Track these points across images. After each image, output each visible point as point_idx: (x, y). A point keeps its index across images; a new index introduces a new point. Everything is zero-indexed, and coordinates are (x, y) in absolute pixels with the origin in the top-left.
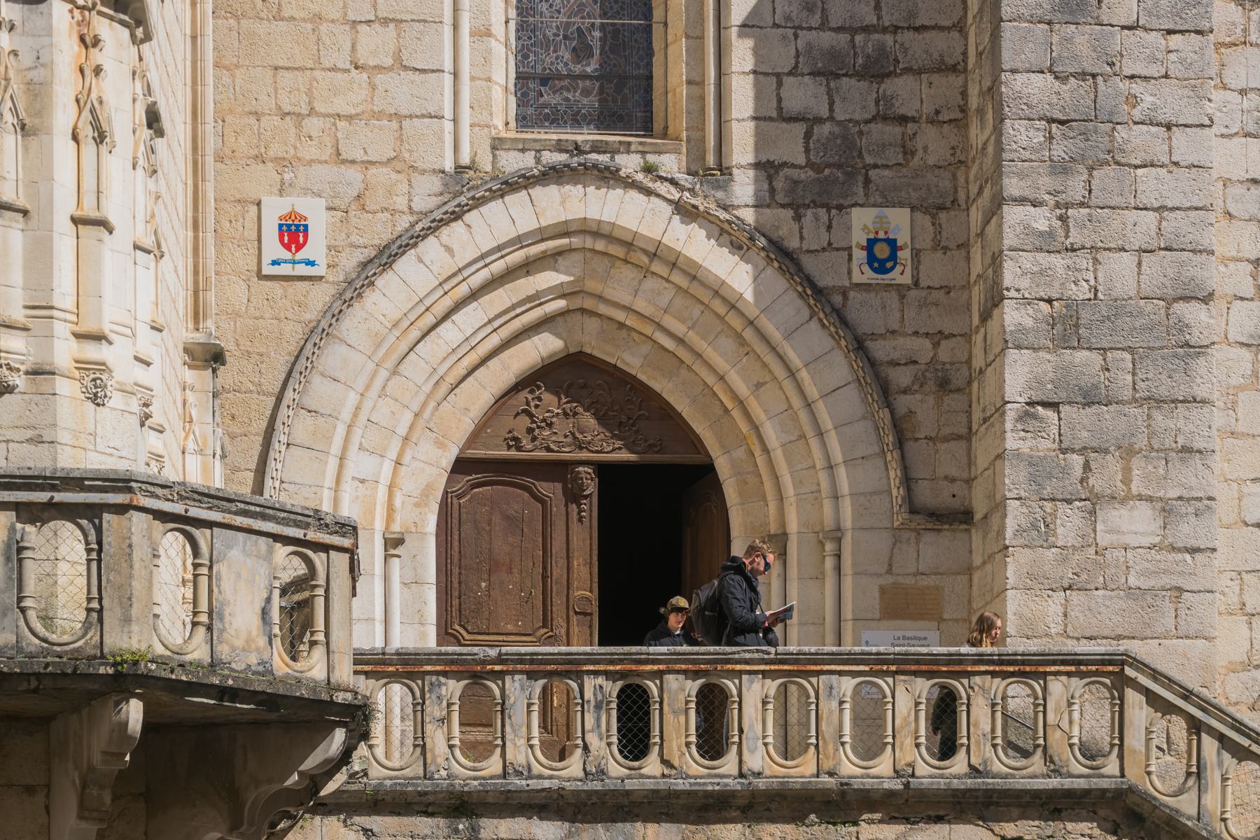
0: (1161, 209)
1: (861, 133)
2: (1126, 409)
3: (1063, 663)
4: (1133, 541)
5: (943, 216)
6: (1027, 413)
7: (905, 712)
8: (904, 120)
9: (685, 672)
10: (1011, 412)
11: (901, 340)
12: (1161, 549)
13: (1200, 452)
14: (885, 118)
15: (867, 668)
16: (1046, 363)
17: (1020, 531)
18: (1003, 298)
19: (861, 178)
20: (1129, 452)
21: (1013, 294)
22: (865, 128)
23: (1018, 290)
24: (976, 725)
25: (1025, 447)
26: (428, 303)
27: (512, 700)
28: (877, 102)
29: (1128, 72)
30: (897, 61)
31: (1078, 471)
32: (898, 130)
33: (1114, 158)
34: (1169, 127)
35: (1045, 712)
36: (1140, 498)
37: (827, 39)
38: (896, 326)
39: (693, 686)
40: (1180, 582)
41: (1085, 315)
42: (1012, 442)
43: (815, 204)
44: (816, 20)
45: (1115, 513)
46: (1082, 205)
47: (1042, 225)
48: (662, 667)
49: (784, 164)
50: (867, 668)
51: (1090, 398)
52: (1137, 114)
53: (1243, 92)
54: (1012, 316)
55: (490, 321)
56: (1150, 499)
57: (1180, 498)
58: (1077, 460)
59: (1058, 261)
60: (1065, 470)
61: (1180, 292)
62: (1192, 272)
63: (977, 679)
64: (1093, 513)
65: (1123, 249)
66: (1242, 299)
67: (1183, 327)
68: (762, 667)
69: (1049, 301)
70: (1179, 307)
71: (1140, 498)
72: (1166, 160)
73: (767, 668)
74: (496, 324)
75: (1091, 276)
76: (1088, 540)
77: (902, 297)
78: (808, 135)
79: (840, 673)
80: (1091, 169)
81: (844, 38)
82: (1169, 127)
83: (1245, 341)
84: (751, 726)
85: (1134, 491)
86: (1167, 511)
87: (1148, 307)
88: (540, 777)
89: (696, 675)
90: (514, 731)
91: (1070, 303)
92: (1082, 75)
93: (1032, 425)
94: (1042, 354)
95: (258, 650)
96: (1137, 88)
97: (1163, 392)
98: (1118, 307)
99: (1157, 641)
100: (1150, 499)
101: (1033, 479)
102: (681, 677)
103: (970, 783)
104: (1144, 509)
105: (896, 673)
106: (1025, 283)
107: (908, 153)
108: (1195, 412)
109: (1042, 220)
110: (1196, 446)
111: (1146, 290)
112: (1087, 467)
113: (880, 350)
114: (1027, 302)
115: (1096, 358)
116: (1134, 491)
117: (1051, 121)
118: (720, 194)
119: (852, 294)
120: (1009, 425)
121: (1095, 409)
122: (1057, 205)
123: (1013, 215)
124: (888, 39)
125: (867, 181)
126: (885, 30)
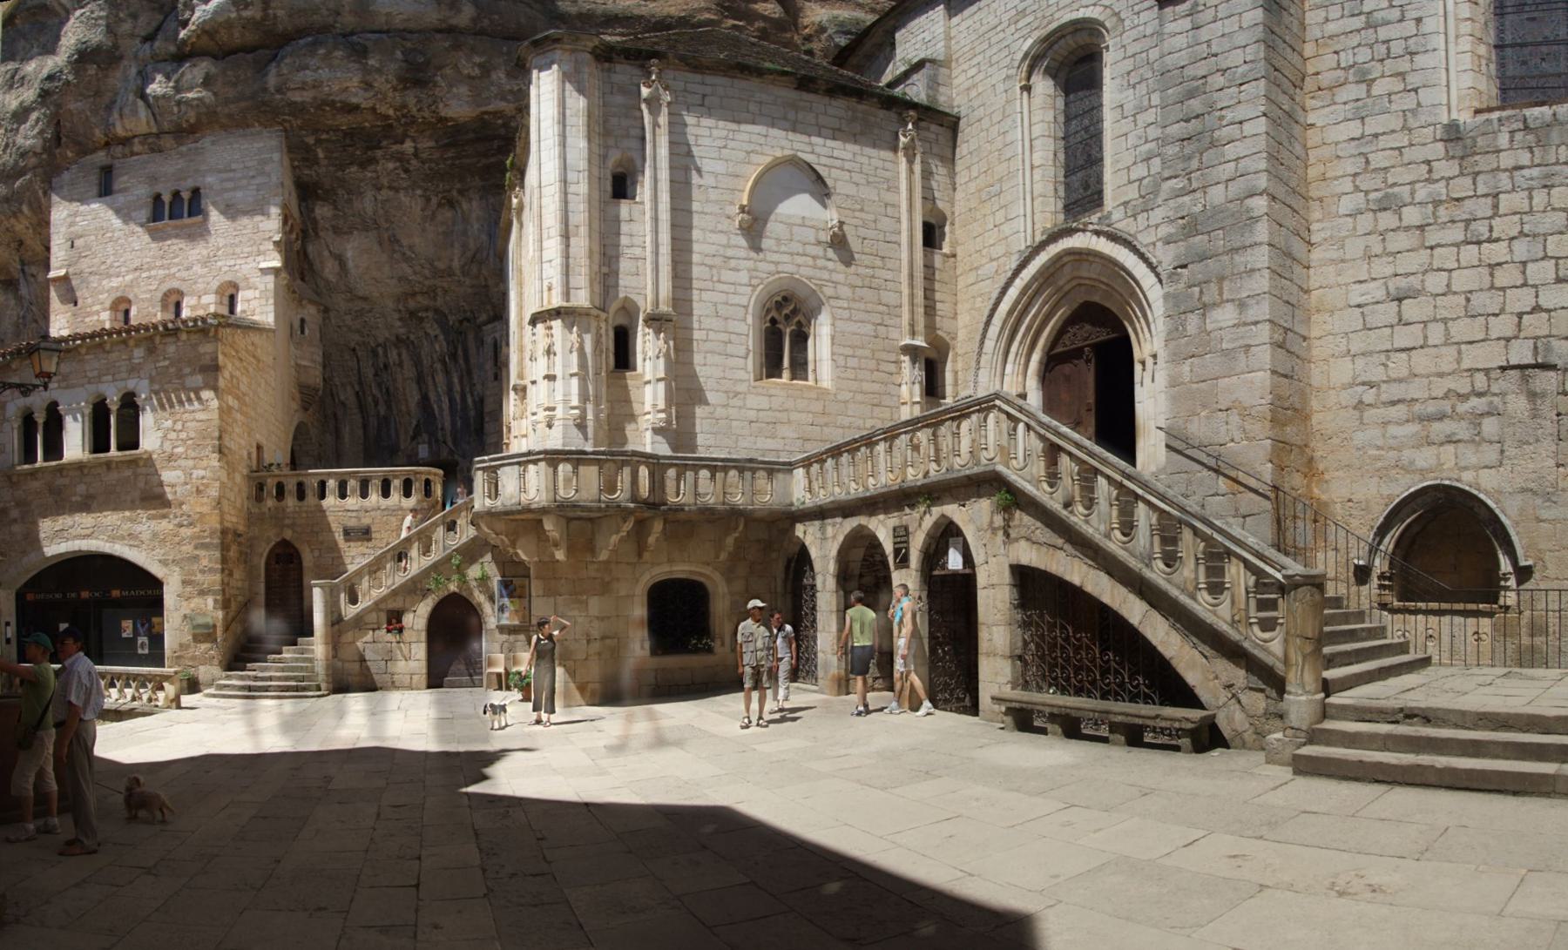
4: (1223, 324)
20: (1221, 279)
41: (1200, 219)
51: (1203, 258)
52: (1224, 123)
53: (1345, 103)
60: (1191, 296)
64: (1204, 315)
71: (1228, 301)
87: (1231, 206)
112: (1201, 292)
115: (1206, 237)
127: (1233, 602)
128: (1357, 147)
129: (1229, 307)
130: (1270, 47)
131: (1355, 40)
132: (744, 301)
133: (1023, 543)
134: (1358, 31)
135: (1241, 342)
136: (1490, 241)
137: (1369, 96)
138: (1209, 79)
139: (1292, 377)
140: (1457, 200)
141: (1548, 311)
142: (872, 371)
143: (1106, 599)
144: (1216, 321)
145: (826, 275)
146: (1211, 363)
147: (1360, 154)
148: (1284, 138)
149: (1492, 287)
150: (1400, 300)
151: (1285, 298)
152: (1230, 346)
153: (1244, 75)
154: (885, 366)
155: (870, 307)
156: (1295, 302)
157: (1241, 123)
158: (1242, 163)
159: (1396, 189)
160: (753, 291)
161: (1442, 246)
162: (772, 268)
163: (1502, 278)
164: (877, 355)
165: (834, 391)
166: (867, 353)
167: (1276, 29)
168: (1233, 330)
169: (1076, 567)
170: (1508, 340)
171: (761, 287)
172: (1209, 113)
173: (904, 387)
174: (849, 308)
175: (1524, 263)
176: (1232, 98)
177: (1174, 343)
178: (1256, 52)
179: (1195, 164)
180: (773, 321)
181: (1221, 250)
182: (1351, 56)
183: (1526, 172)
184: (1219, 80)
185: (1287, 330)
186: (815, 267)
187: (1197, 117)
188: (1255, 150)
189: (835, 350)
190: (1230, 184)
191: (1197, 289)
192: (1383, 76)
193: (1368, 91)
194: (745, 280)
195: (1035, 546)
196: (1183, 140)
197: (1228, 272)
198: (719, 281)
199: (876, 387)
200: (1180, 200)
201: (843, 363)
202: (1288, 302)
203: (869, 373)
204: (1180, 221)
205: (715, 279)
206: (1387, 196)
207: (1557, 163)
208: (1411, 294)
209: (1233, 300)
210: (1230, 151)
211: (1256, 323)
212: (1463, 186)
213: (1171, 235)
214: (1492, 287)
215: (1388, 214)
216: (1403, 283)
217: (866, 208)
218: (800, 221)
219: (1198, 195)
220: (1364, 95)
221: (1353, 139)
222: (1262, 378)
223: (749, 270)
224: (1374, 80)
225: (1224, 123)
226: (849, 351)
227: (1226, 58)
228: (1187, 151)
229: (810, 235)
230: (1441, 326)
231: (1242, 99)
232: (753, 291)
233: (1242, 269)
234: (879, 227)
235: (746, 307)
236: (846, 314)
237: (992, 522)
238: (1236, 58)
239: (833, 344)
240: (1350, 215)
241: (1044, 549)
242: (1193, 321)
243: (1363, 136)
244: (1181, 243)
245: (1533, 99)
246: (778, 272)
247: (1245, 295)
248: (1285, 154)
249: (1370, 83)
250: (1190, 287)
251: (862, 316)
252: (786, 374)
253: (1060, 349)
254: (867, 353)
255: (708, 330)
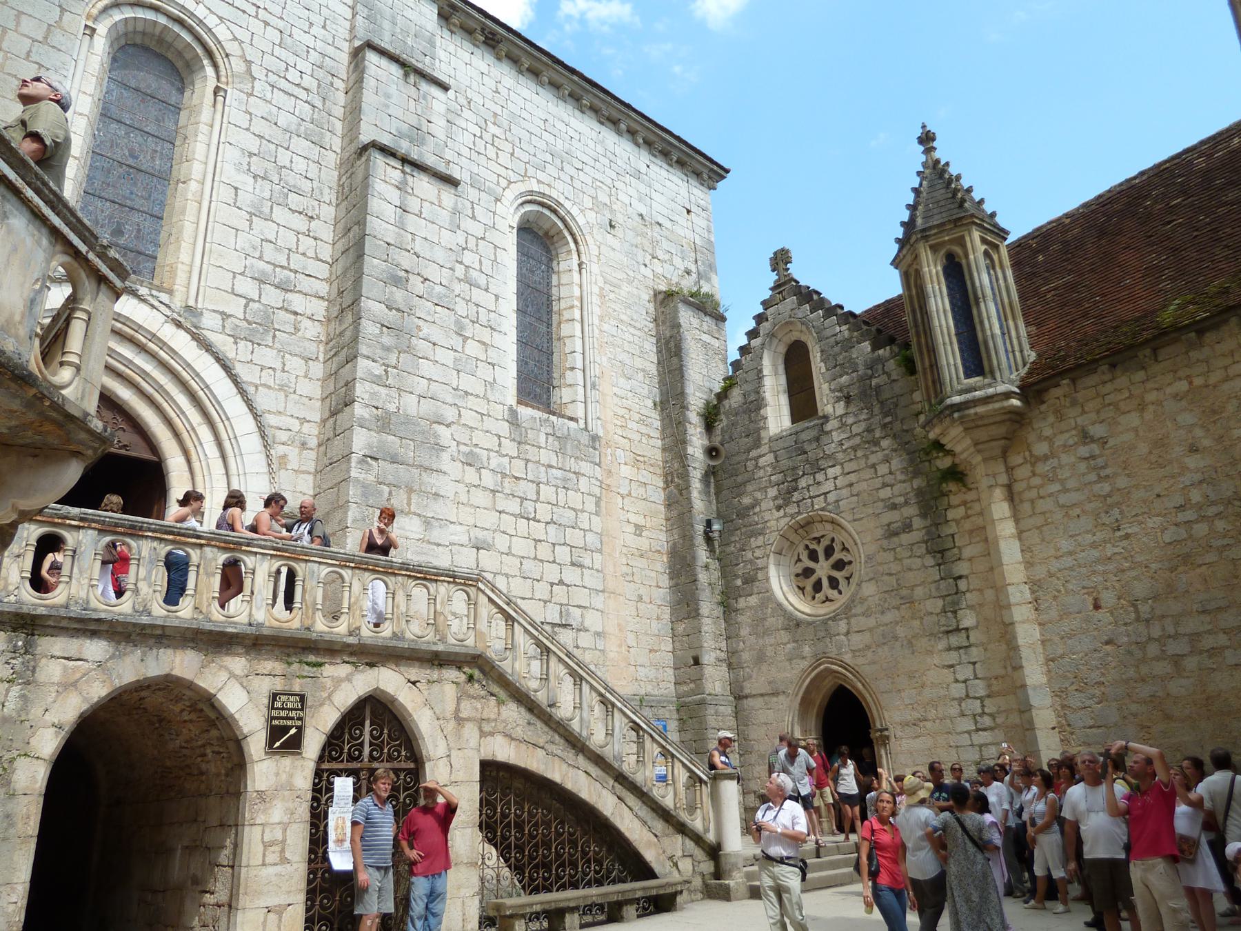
0: (430, 379)
1: (274, 313)
2: (410, 468)
3: (447, 576)
5: (311, 362)
6: (363, 460)
7: (357, 593)
8: (296, 313)
9: (219, 547)
10: (354, 459)
11: (284, 417)
14: (287, 310)
15: (337, 563)
16: (374, 437)
17: (355, 521)
18: (354, 401)
19: (272, 334)
20: (410, 491)
21: (359, 400)
22: (276, 311)
24: (398, 607)
25: (362, 477)
27: (83, 549)
28: (284, 301)
30: (295, 286)
31: (386, 495)
32: (293, 317)
33: (409, 349)
34: (434, 344)
35: (435, 604)
36: (414, 514)
37: (261, 265)
38: (282, 410)
39: (222, 557)
41: (393, 419)
42: (354, 473)
43: (246, 339)
44: (257, 255)
46: (395, 367)
47: (377, 373)
48: (203, 542)
49: (231, 316)
50: (337, 563)
52: (421, 334)
54: (358, 410)
56: (419, 515)
58: (386, 489)
59: (383, 390)
60: (380, 493)
61: (436, 419)
62: (442, 412)
63: (400, 578)
65: (411, 393)
67: (436, 436)
68: (272, 552)
69: (377, 408)
70: (435, 426)
71: (414, 514)
72: (432, 358)
73: (275, 553)
75: (396, 401)
77: (287, 396)
78: (246, 306)
79: (320, 563)
80: (400, 352)
81: (269, 268)
82: (434, 344)
84: (260, 591)
85: (412, 510)
86: (427, 523)
87: (423, 423)
88: (95, 610)
89: (226, 549)
90: (81, 572)
91: (387, 412)
92: (398, 310)
93: (365, 467)
94: (372, 433)
95: (17, 337)
96: (421, 323)
97: (426, 464)
98: (408, 421)
100: (419, 515)
101: (364, 495)
102: (215, 550)
103: (394, 643)
104: (416, 520)
105: (353, 568)
106: (366, 396)
107: (297, 329)
108: (441, 476)
109: (378, 370)
110: (442, 494)
111: (422, 414)
112: (390, 493)
113: (271, 420)
114: (367, 406)
115: (397, 440)
117: (383, 325)
118: (194, 320)
119: (260, 388)
120: (353, 464)
121: (395, 465)
122: (384, 364)
123: (362, 364)
124: (292, 275)
125: (274, 337)
126: (291, 270)
127: (675, 794)
133: (499, 739)
136: (534, 520)
140: (516, 478)
141: (568, 586)
143: (584, 795)
149: (535, 558)
150: (478, 549)
158: (434, 386)
159: (477, 450)
161: (507, 513)
163: (544, 552)
169: (557, 766)
170: (545, 602)
175: (554, 544)
183: (554, 471)
195: (513, 743)
206: (471, 452)
207: (570, 471)
208: (486, 546)
210: (426, 367)
212: (518, 468)
214: (535, 558)
215: (472, 469)
216: (481, 534)
230: (504, 578)
237: (457, 710)
241: (523, 746)
245: (61, 344)
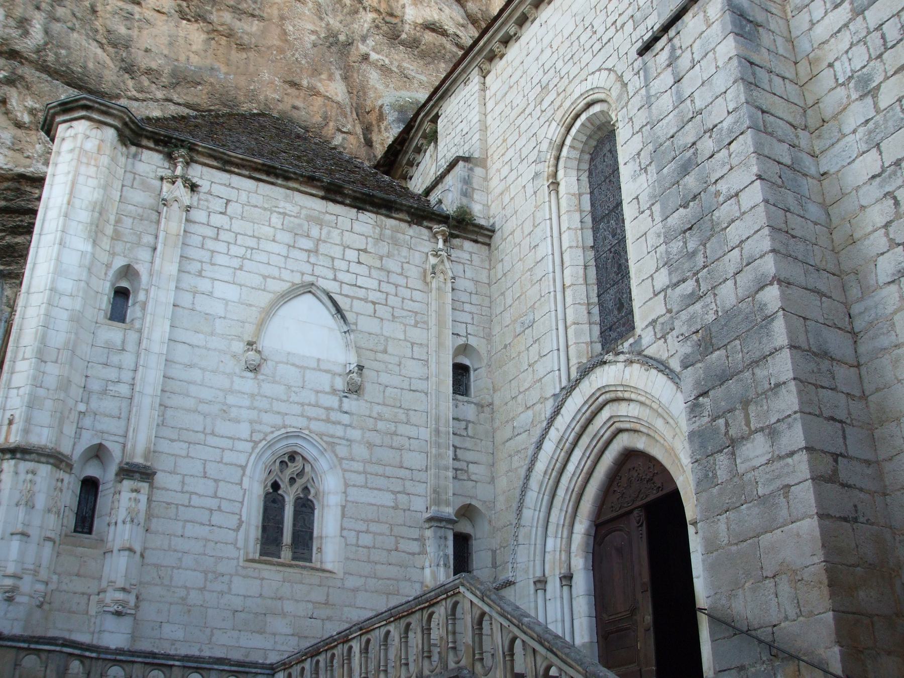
4: (757, 463)
12: (773, 462)
13: (784, 383)
20: (746, 403)
23: (682, 335)
26: (556, 457)
29: (713, 180)
40: (787, 481)
45: (744, 448)
51: (723, 378)
52: (721, 199)
53: (854, 132)
55: (584, 454)
57: (778, 421)
60: (716, 431)
64: (733, 454)
66: (882, 254)
71: (756, 431)
74: (587, 454)
76: (734, 473)
83: (890, 280)
85: (753, 428)
87: (743, 306)
99: (779, 530)
112: (727, 424)
115: (722, 352)
116: (753, 428)
128: (881, 186)
129: (760, 438)
130: (751, 84)
131: (845, 39)
132: (242, 460)
134: (846, 25)
135: (778, 483)
137: (878, 111)
138: (699, 145)
139: (856, 520)
142: (389, 551)
144: (748, 460)
145: (339, 431)
146: (750, 515)
147: (885, 195)
148: (791, 200)
151: (827, 413)
152: (767, 491)
153: (730, 131)
154: (404, 545)
155: (389, 471)
156: (843, 418)
157: (737, 195)
160: (253, 448)
162: (278, 420)
164: (396, 530)
165: (341, 575)
166: (384, 528)
167: (756, 58)
168: (769, 468)
171: (264, 443)
172: (705, 190)
173: (427, 572)
174: (365, 472)
176: (724, 164)
177: (704, 494)
178: (736, 95)
179: (700, 260)
180: (276, 486)
181: (740, 366)
182: (847, 64)
184: (707, 145)
185: (836, 457)
186: (328, 421)
187: (694, 198)
188: (756, 228)
189: (345, 525)
190: (738, 278)
191: (721, 421)
192: (887, 78)
193: (875, 105)
194: (245, 434)
196: (684, 232)
197: (752, 394)
198: (213, 434)
199: (393, 571)
200: (691, 309)
201: (354, 541)
202: (832, 419)
203: (385, 553)
204: (695, 337)
205: (208, 431)
209: (762, 429)
211: (792, 454)
213: (687, 356)
217: (390, 350)
218: (315, 365)
219: (709, 299)
220: (872, 113)
221: (874, 177)
222: (809, 527)
223: (251, 422)
224: (878, 87)
225: (721, 199)
226: (362, 527)
227: (710, 113)
228: (691, 246)
229: (325, 381)
231: (734, 162)
232: (253, 448)
233: (767, 386)
234: (403, 372)
235: (244, 468)
236: (360, 479)
238: (718, 113)
239: (343, 516)
240: (893, 282)
242: (722, 460)
243: (883, 170)
244: (699, 365)
246: (285, 427)
247: (773, 420)
248: (795, 222)
249: (874, 93)
250: (714, 420)
251: (381, 482)
252: (286, 554)
253: (600, 520)
254: (384, 528)
255: (192, 493)
